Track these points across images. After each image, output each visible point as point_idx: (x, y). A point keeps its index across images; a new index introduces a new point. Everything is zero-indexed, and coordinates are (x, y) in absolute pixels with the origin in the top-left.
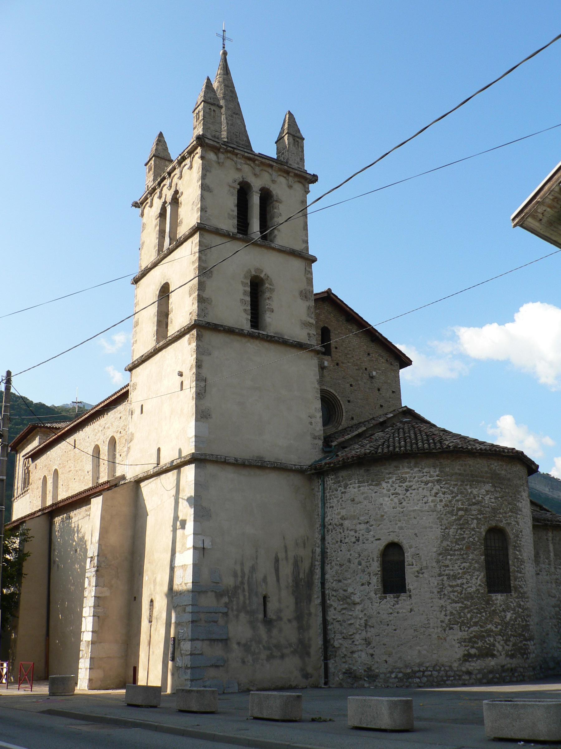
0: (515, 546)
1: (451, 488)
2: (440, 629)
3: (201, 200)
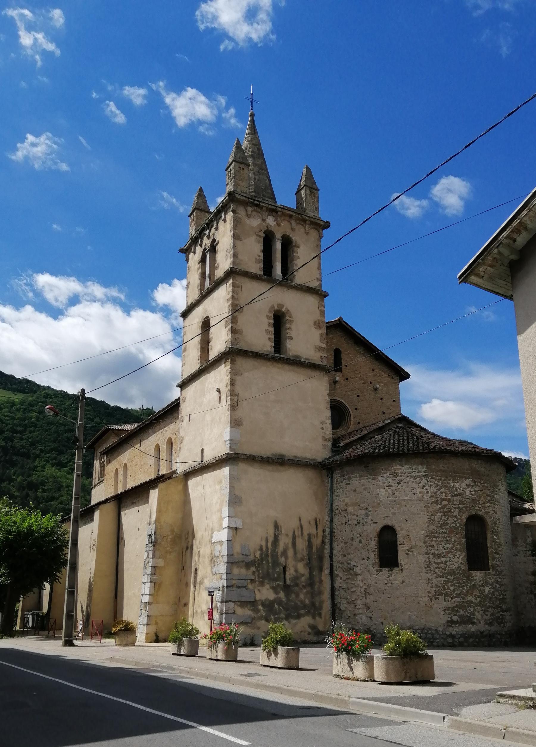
0: (493, 532)
1: (436, 482)
2: (427, 599)
3: (233, 248)
